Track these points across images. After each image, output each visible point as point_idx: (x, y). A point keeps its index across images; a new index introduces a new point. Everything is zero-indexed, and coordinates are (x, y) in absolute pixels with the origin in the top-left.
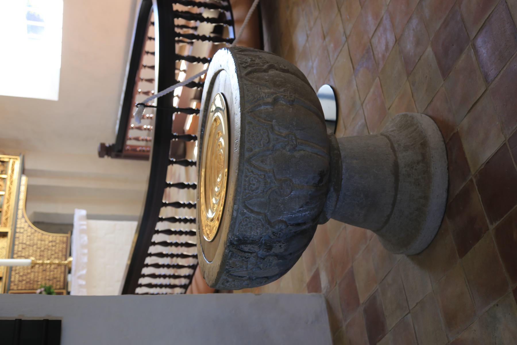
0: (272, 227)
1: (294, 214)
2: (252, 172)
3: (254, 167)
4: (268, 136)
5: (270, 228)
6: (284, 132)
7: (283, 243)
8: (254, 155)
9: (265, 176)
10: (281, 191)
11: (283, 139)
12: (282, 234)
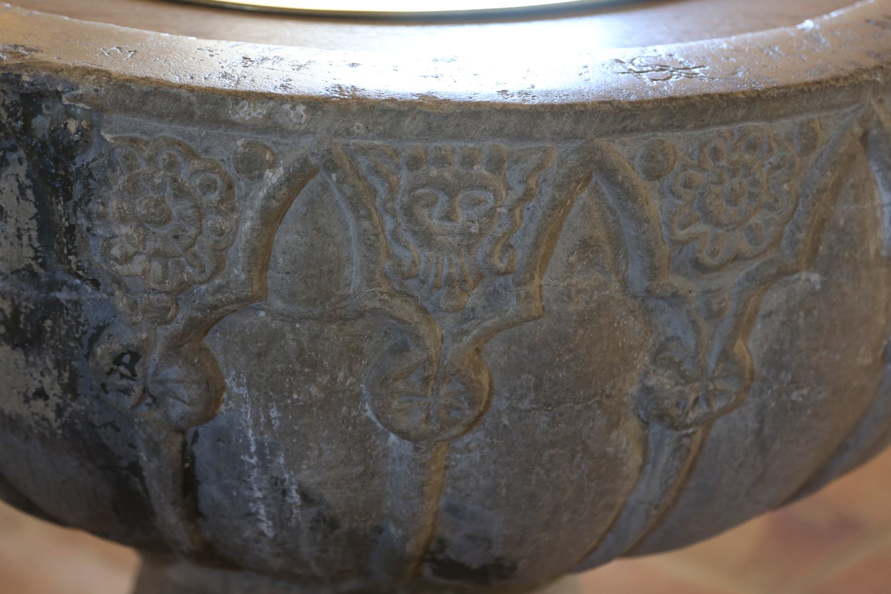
0: (175, 346)
1: (264, 464)
2: (527, 195)
3: (558, 207)
4: (738, 258)
5: (163, 332)
6: (751, 349)
7: (59, 411)
8: (627, 194)
9: (506, 273)
10: (413, 378)
11: (717, 347)
12: (128, 402)
